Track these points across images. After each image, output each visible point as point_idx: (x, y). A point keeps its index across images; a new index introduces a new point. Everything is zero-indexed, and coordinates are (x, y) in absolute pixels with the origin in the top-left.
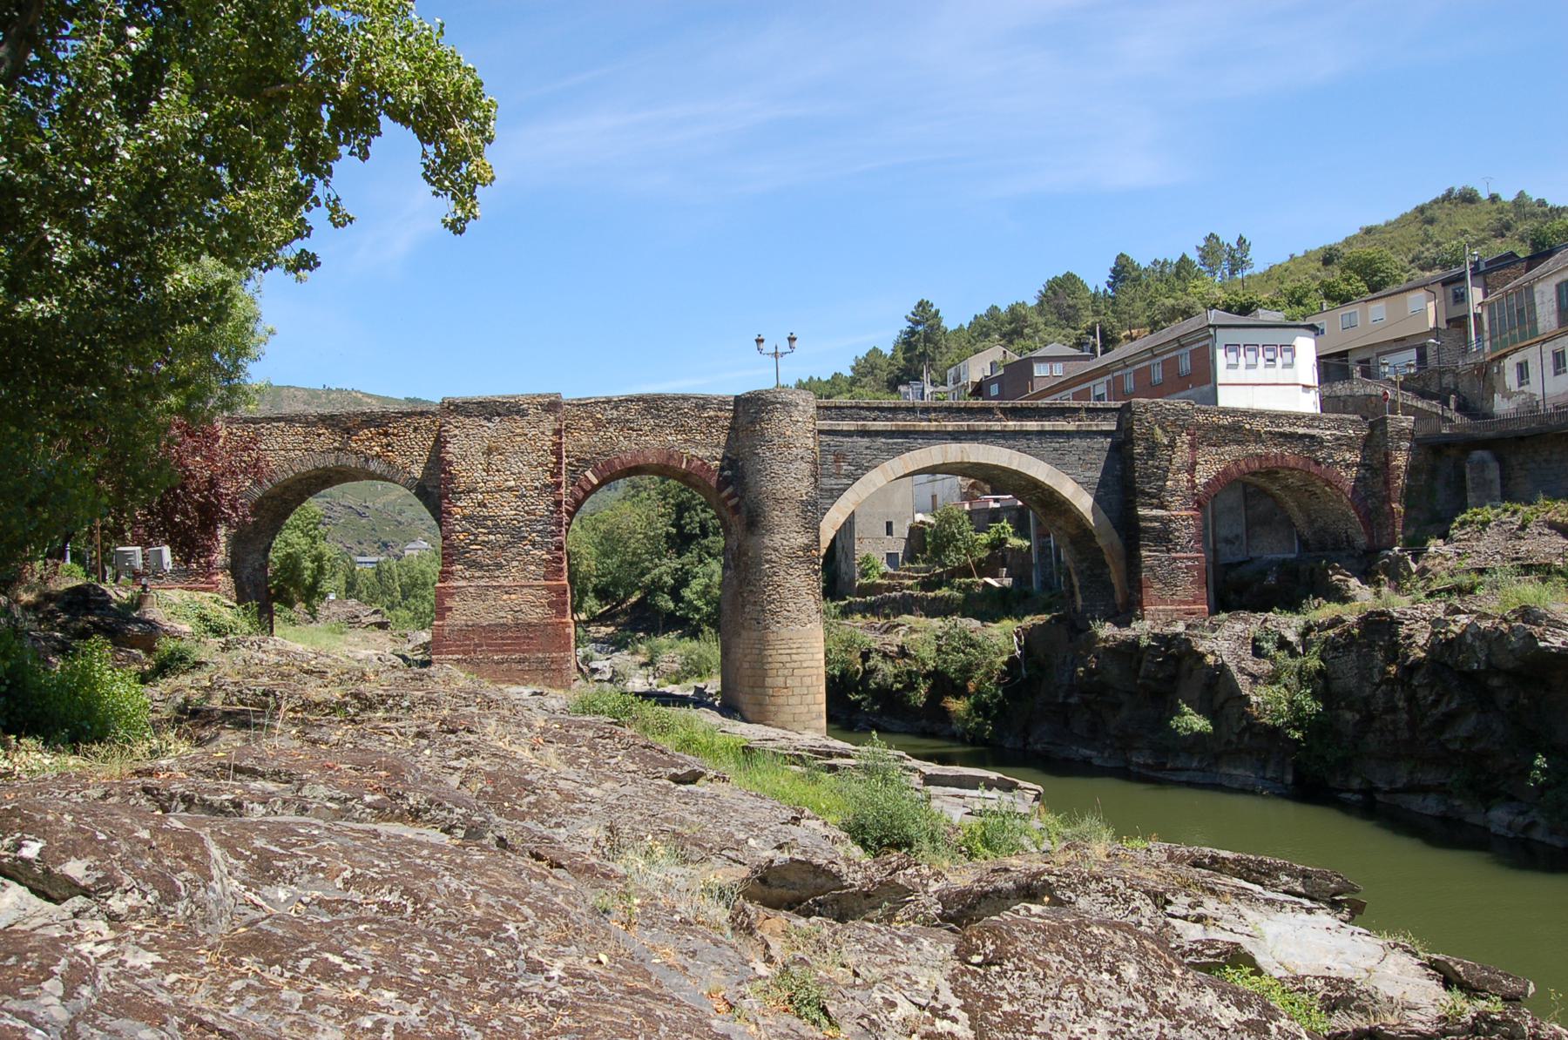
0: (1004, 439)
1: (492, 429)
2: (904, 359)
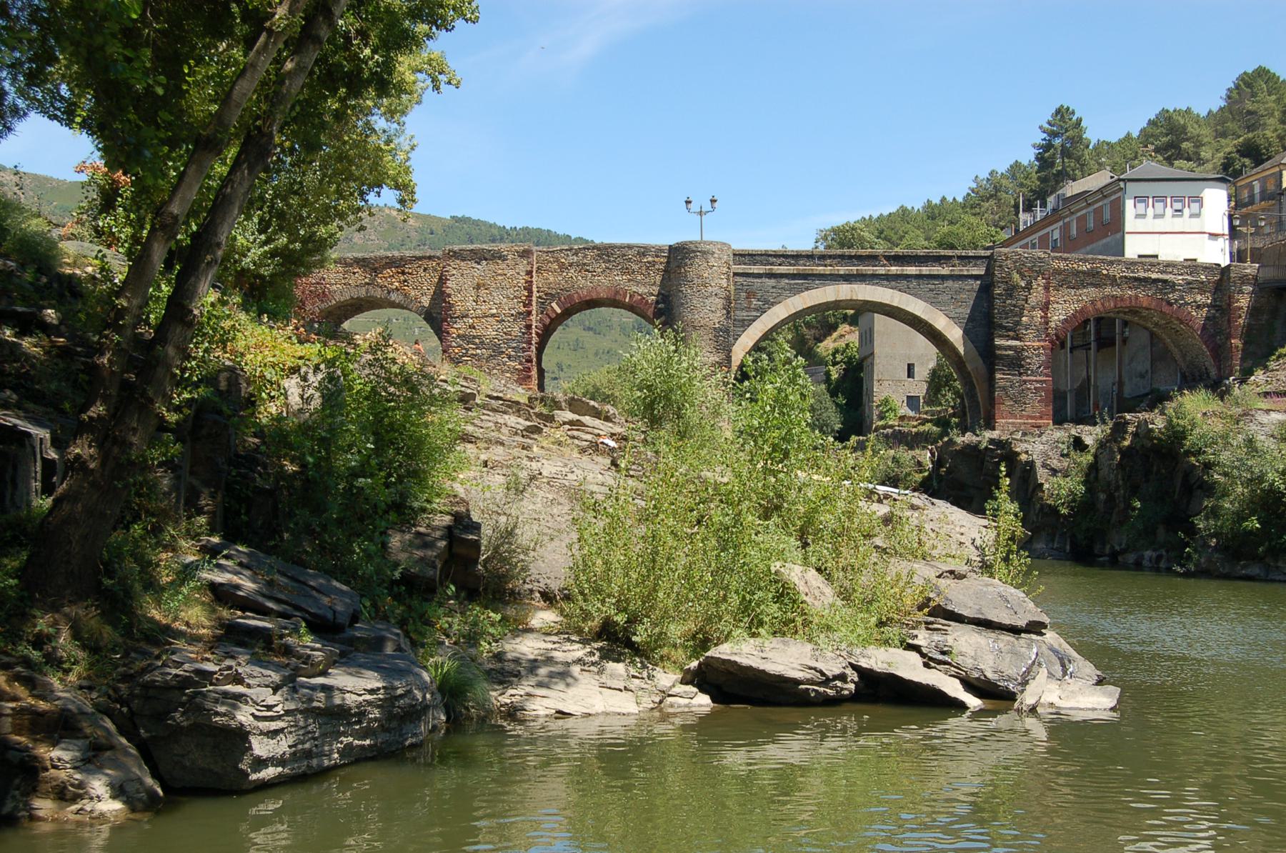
0: (888, 280)
1: (480, 270)
2: (1039, 178)
